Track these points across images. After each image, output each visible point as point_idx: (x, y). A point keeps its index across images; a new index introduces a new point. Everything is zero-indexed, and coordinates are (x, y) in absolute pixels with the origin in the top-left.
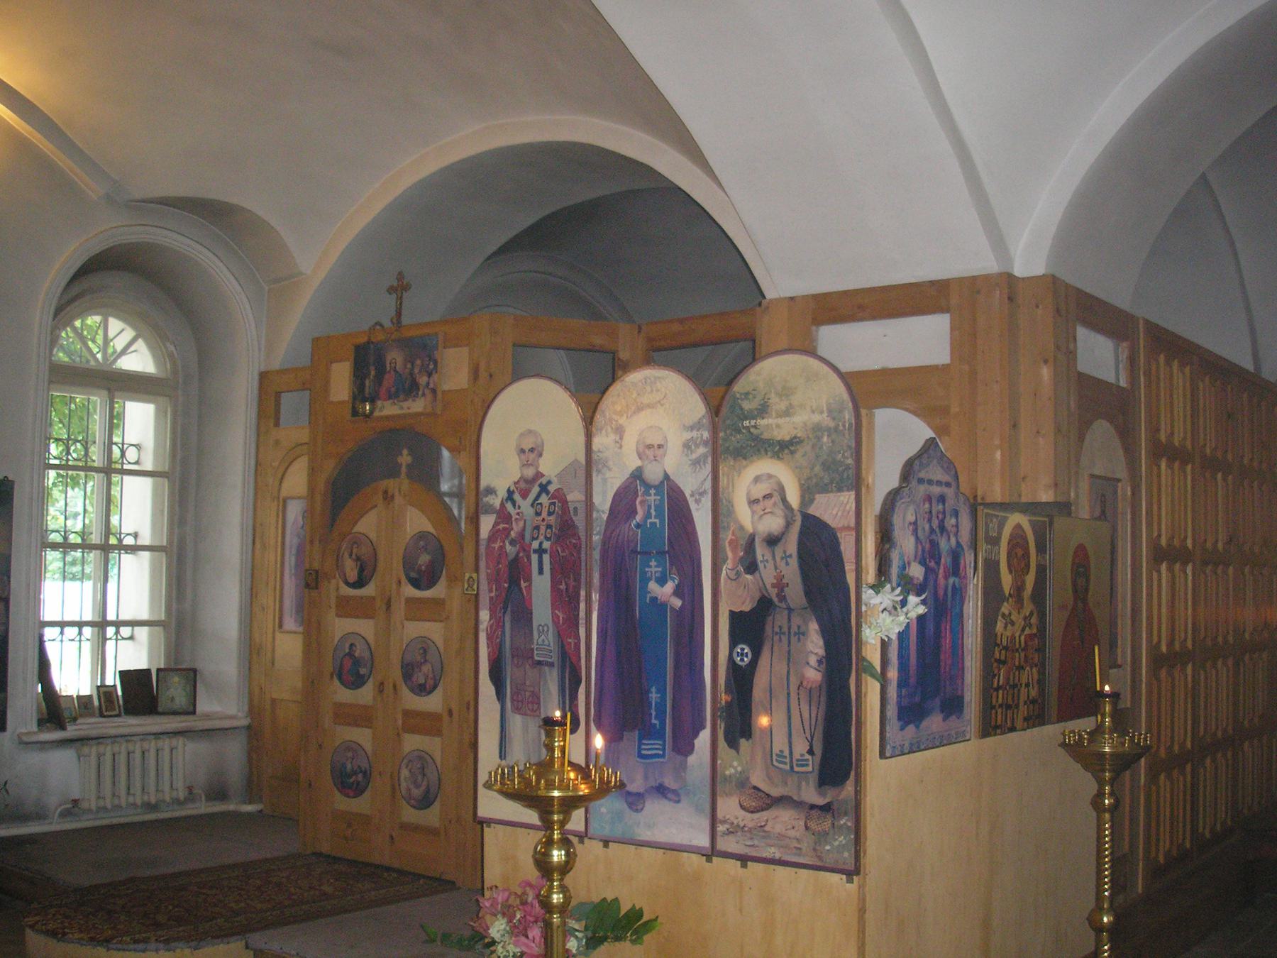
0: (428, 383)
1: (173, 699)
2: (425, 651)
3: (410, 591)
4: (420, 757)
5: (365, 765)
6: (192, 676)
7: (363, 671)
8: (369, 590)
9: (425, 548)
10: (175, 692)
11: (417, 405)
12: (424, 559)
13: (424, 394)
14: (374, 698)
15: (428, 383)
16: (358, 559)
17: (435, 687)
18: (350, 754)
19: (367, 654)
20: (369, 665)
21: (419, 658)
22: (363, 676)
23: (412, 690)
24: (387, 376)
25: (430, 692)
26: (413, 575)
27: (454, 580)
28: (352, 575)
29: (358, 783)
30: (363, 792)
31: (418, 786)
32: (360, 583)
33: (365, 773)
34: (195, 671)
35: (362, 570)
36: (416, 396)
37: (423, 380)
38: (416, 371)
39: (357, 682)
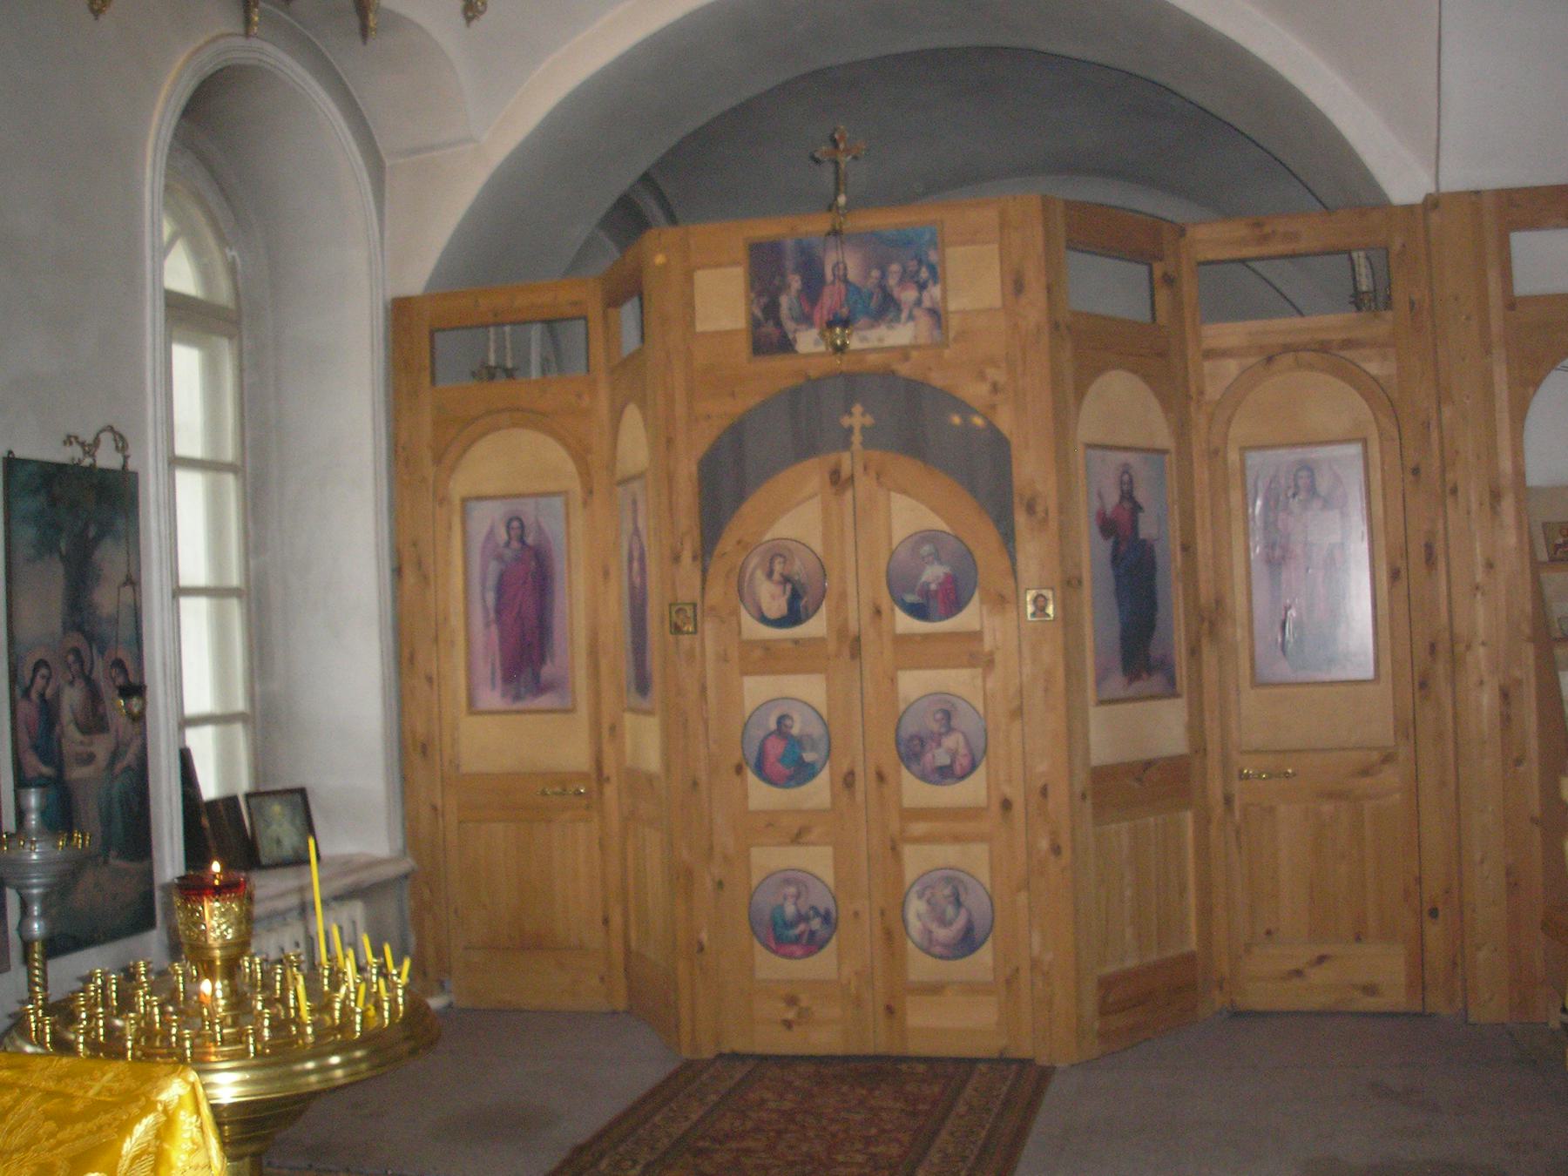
0: (919, 302)
1: (279, 842)
2: (948, 715)
3: (905, 623)
4: (949, 880)
5: (824, 903)
6: (299, 799)
7: (809, 756)
8: (815, 626)
9: (937, 558)
10: (278, 829)
11: (900, 335)
12: (933, 574)
13: (911, 317)
14: (834, 796)
15: (919, 302)
16: (786, 579)
17: (973, 767)
18: (792, 890)
19: (817, 730)
20: (823, 746)
21: (935, 727)
22: (812, 765)
23: (924, 777)
24: (827, 291)
25: (963, 777)
26: (911, 598)
27: (1001, 602)
28: (776, 605)
29: (812, 933)
30: (821, 947)
31: (944, 922)
32: (794, 616)
33: (826, 918)
34: (302, 792)
35: (795, 597)
36: (897, 319)
37: (908, 295)
38: (892, 281)
39: (801, 773)
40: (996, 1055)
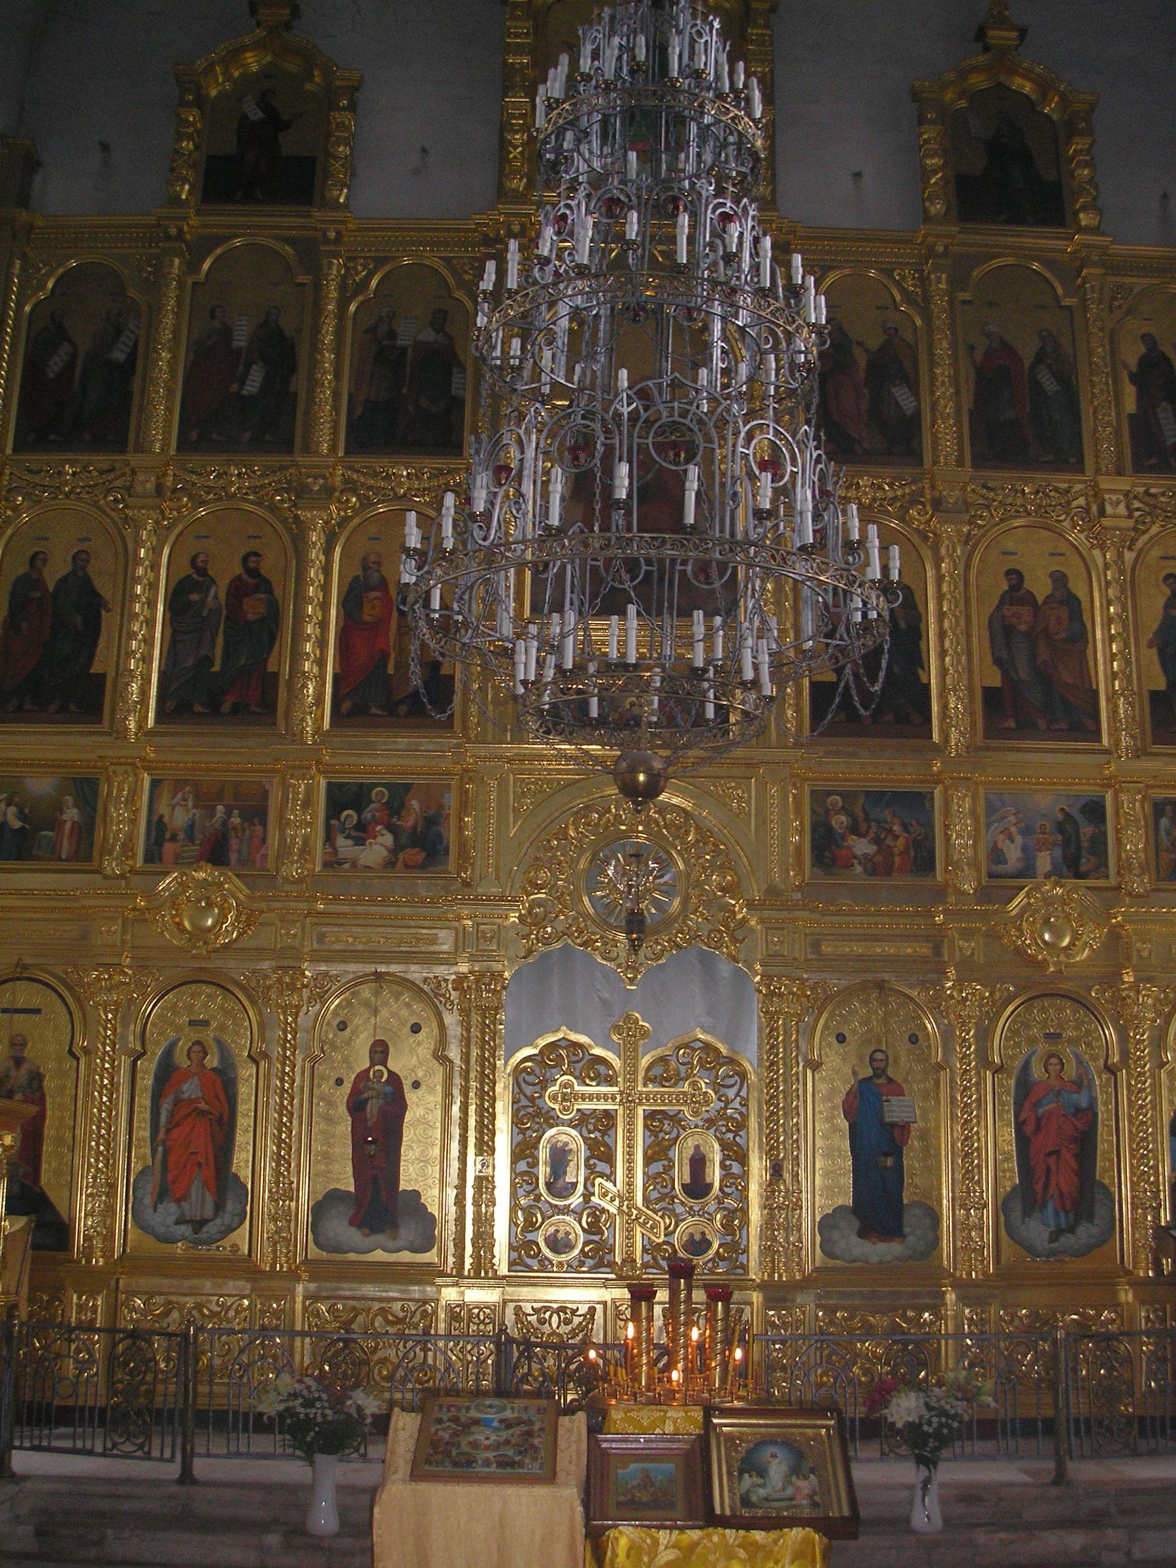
40: (409, 1177)
